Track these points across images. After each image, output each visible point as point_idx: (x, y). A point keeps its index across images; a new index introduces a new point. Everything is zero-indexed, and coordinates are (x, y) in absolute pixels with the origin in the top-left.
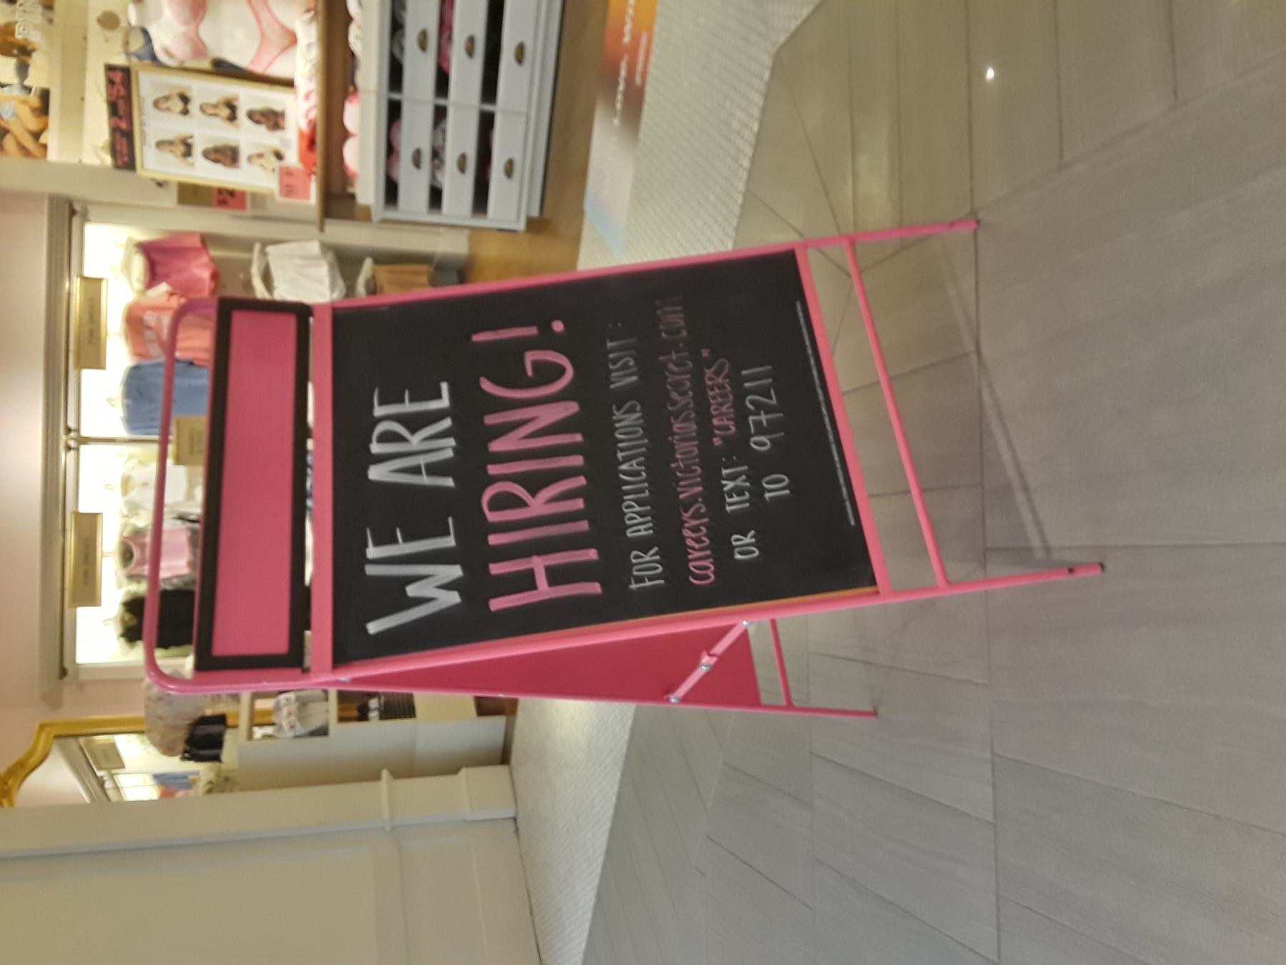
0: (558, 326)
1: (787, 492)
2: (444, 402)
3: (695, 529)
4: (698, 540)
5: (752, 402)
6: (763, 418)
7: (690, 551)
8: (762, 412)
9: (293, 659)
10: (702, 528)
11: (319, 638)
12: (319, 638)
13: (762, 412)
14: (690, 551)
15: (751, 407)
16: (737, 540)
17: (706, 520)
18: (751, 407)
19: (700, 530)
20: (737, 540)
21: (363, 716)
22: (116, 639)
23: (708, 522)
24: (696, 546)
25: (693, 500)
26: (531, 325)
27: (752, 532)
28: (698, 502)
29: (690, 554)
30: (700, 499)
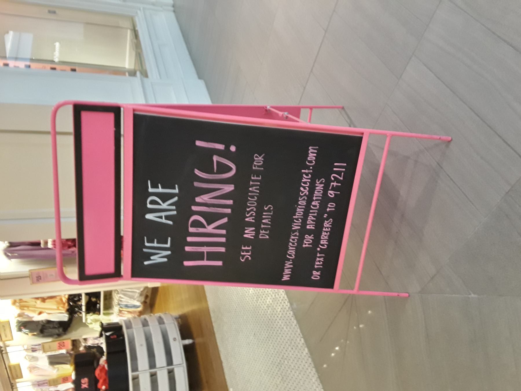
0: (233, 148)
1: (334, 209)
2: (168, 245)
3: (293, 240)
4: (293, 244)
5: (334, 177)
6: (335, 184)
7: (304, 178)
8: (335, 182)
9: (117, 274)
10: (308, 183)
11: (126, 266)
12: (126, 266)
13: (335, 182)
14: (304, 178)
15: (333, 179)
16: (307, 237)
17: (297, 238)
18: (333, 179)
19: (295, 240)
20: (307, 237)
21: (183, 337)
22: (15, 326)
23: (293, 267)
24: (306, 177)
25: (295, 231)
26: (220, 260)
27: (312, 235)
28: (297, 232)
29: (303, 179)
30: (298, 231)
